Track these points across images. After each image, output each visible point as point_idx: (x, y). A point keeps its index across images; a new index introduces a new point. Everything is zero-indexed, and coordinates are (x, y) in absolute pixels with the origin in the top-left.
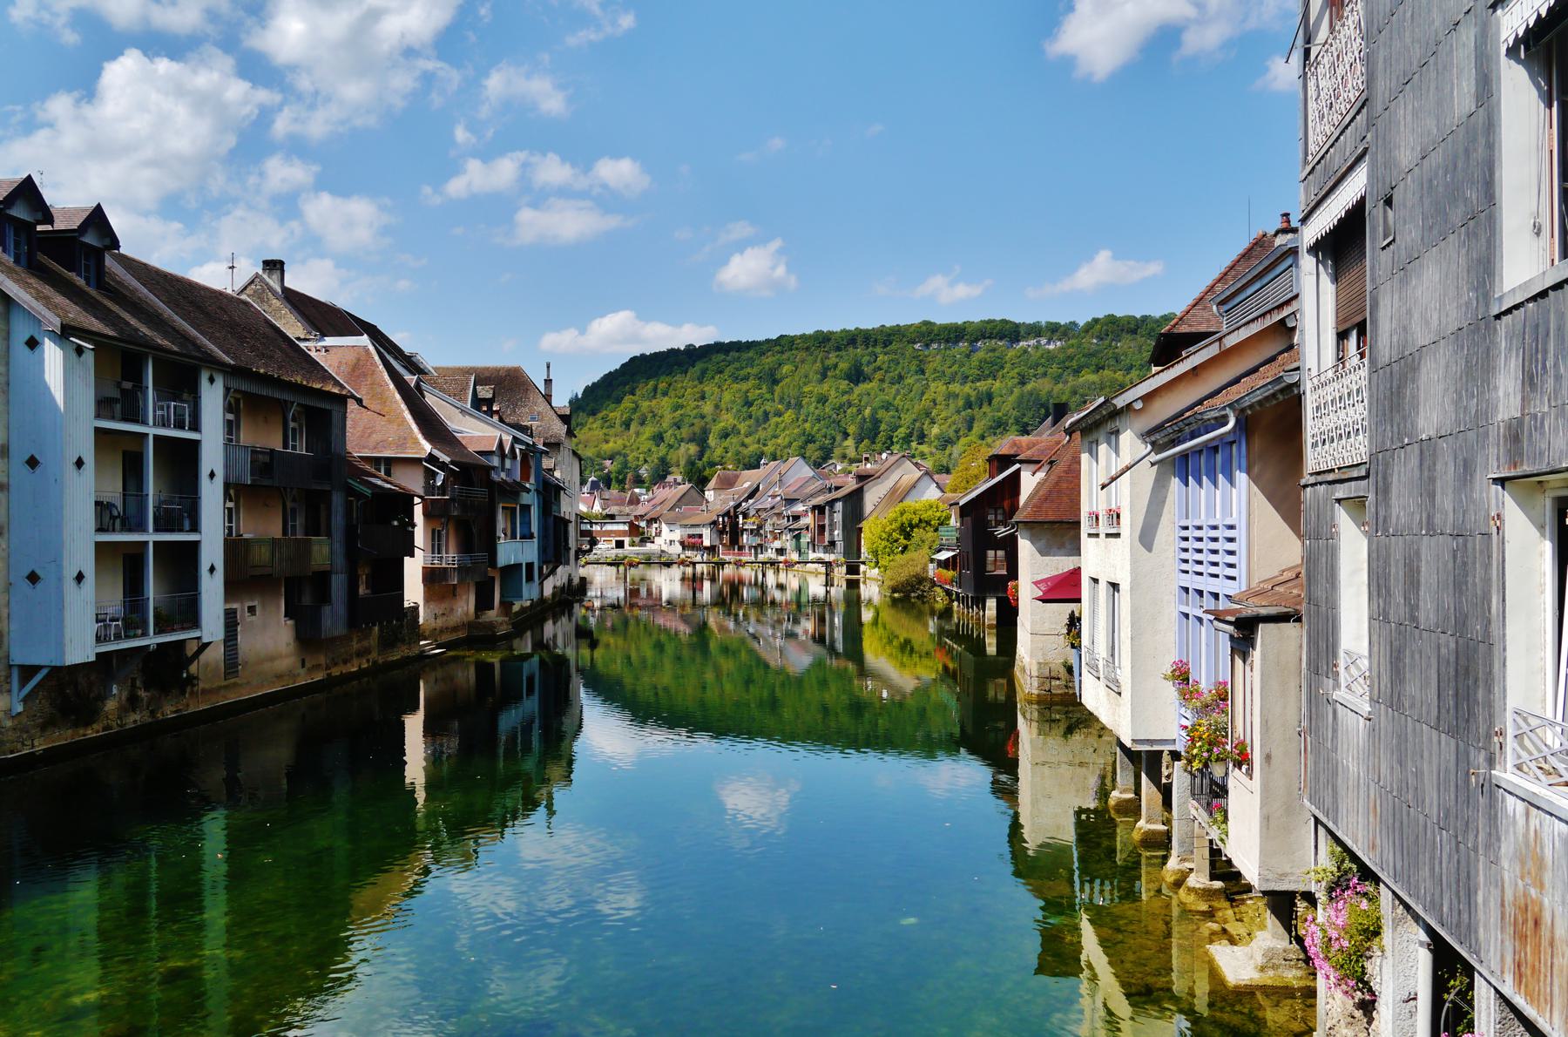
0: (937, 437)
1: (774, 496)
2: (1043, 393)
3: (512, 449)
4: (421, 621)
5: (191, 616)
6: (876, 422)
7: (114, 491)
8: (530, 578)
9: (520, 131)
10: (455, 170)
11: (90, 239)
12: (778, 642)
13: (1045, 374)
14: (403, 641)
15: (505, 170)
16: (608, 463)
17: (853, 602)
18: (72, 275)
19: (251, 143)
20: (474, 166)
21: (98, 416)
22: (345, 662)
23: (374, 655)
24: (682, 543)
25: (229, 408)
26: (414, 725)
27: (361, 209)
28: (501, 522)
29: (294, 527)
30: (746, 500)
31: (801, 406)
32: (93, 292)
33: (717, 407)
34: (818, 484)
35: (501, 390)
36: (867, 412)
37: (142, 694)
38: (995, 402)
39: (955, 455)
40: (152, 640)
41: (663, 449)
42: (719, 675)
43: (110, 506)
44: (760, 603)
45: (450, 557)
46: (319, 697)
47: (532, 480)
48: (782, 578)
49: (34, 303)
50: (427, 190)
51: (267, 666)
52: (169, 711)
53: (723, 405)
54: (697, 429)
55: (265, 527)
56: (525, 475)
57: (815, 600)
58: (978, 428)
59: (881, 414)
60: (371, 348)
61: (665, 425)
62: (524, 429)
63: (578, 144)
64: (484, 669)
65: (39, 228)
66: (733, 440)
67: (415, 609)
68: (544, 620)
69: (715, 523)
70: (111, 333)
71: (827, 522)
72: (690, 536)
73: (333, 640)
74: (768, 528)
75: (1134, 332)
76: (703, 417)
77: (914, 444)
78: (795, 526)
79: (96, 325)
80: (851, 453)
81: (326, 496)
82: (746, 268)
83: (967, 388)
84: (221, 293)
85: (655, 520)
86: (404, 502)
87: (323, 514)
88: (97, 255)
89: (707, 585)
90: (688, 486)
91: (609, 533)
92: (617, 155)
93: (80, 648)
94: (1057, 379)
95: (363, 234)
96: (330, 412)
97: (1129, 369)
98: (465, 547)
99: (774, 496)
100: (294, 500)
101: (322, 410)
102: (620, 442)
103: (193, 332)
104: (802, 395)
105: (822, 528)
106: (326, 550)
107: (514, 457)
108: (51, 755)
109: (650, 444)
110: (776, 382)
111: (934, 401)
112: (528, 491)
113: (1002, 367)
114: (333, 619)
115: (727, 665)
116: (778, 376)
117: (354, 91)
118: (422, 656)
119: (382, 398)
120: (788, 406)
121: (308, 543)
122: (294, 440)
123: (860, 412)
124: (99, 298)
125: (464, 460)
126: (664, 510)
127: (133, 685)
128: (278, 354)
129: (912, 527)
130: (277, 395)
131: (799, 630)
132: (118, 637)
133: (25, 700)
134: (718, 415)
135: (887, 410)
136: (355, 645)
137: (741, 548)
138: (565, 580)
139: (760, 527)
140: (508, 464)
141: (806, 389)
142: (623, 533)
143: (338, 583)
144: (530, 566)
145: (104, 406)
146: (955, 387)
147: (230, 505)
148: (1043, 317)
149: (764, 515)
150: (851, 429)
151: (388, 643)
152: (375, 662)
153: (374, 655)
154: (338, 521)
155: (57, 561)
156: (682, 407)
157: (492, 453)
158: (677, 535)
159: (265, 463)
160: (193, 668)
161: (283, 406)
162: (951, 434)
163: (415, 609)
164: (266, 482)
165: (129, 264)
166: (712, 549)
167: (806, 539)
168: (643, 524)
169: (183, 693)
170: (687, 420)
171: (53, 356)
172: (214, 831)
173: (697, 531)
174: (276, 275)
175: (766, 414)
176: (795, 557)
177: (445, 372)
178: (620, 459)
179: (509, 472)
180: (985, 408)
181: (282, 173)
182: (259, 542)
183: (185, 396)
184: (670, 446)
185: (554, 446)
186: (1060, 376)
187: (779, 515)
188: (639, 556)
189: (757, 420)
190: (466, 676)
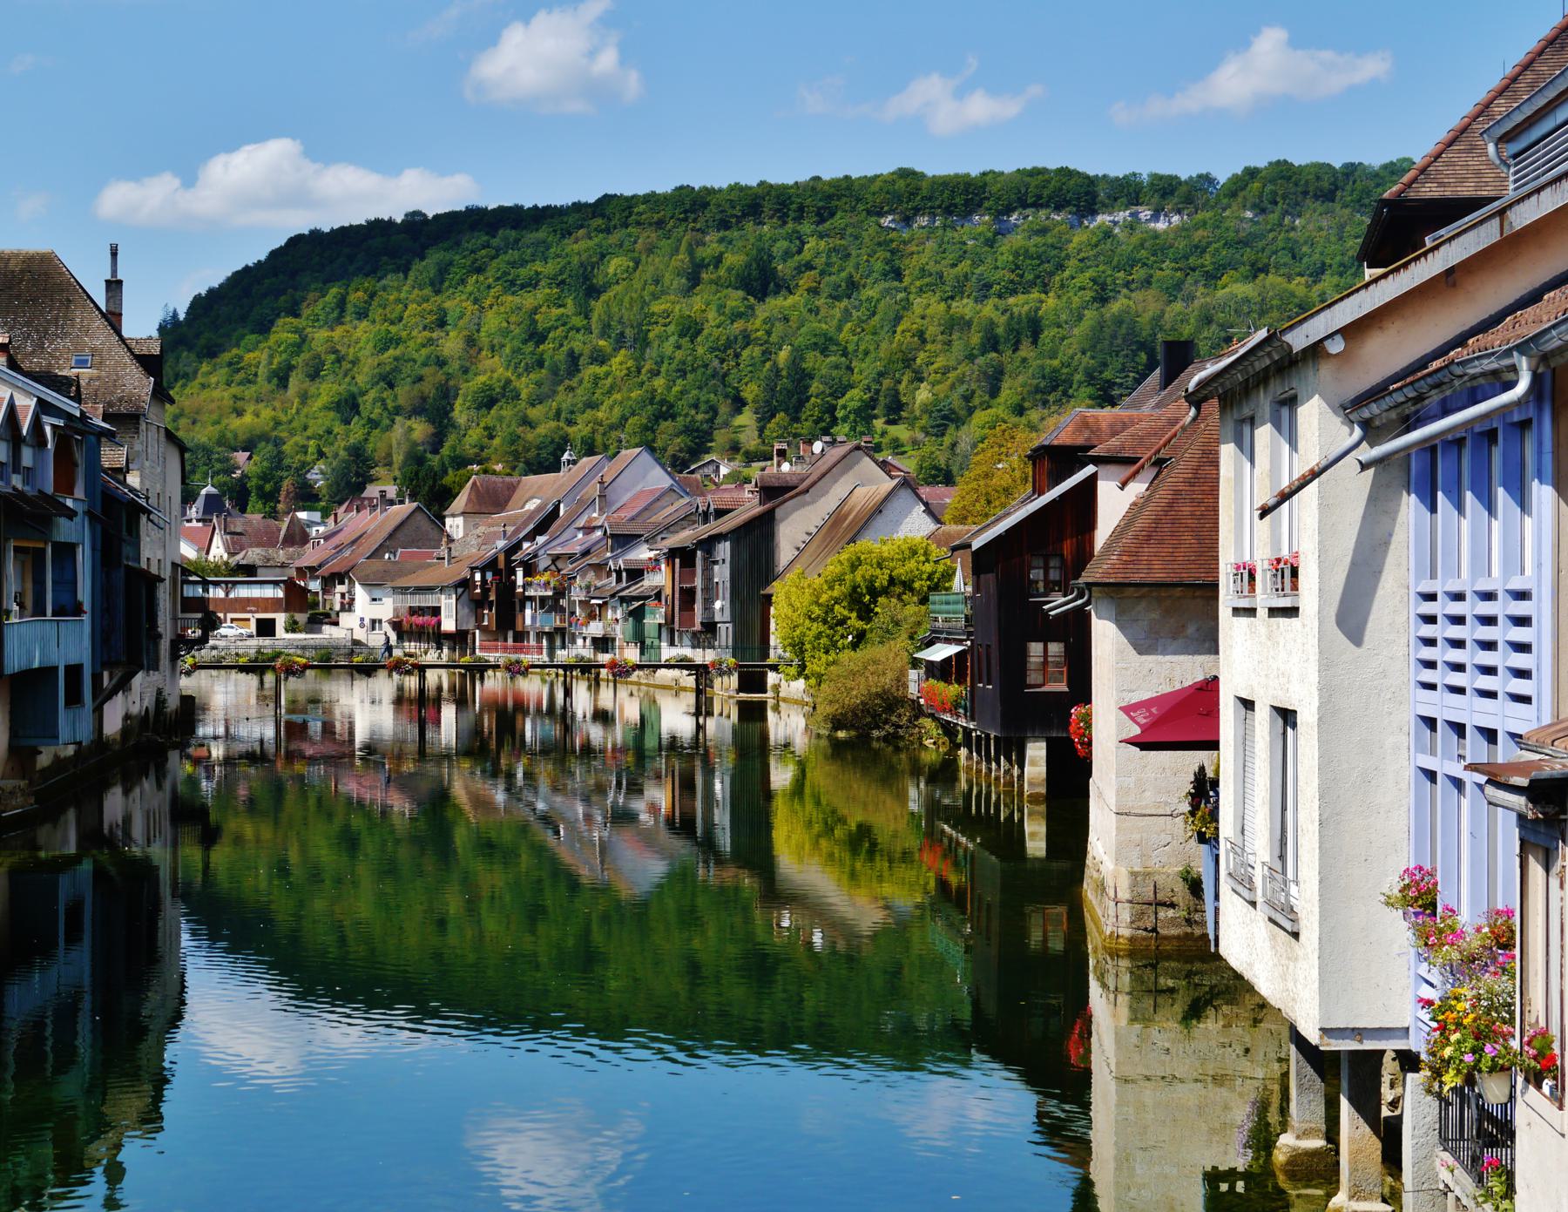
0: (926, 409)
1: (588, 530)
2: (1145, 319)
3: (37, 425)
6: (801, 377)
8: (74, 698)
13: (1147, 282)
16: (241, 457)
17: (752, 745)
21: (68, 668)
24: (396, 625)
30: (531, 537)
31: (646, 343)
33: (471, 342)
34: (681, 504)
36: (783, 356)
38: (1047, 335)
39: (963, 446)
41: (357, 431)
42: (472, 906)
44: (564, 750)
47: (79, 492)
48: (606, 698)
54: (428, 388)
56: (65, 482)
59: (812, 360)
61: (361, 380)
66: (506, 411)
69: (465, 584)
71: (698, 582)
72: (413, 611)
74: (577, 594)
75: (1328, 196)
76: (441, 363)
77: (879, 424)
78: (634, 591)
80: (750, 440)
83: (988, 309)
85: (340, 577)
89: (448, 713)
90: (409, 506)
91: (243, 605)
94: (1173, 291)
97: (1318, 273)
99: (588, 530)
105: (688, 597)
109: (330, 419)
110: (594, 292)
111: (921, 335)
112: (71, 514)
113: (1061, 267)
115: (492, 878)
116: (599, 280)
120: (620, 342)
123: (767, 355)
129: (875, 593)
131: (639, 805)
135: (824, 351)
137: (520, 637)
138: (149, 701)
139: (560, 593)
141: (656, 307)
142: (273, 604)
144: (74, 671)
146: (964, 307)
148: (1144, 164)
149: (567, 568)
150: (750, 391)
156: (398, 341)
158: (386, 609)
162: (956, 402)
166: (460, 639)
167: (655, 618)
168: (315, 586)
170: (407, 369)
173: (428, 601)
175: (573, 358)
176: (632, 655)
178: (266, 449)
179: (28, 474)
180: (1026, 351)
184: (373, 424)
185: (126, 420)
186: (1178, 286)
187: (599, 568)
189: (555, 371)
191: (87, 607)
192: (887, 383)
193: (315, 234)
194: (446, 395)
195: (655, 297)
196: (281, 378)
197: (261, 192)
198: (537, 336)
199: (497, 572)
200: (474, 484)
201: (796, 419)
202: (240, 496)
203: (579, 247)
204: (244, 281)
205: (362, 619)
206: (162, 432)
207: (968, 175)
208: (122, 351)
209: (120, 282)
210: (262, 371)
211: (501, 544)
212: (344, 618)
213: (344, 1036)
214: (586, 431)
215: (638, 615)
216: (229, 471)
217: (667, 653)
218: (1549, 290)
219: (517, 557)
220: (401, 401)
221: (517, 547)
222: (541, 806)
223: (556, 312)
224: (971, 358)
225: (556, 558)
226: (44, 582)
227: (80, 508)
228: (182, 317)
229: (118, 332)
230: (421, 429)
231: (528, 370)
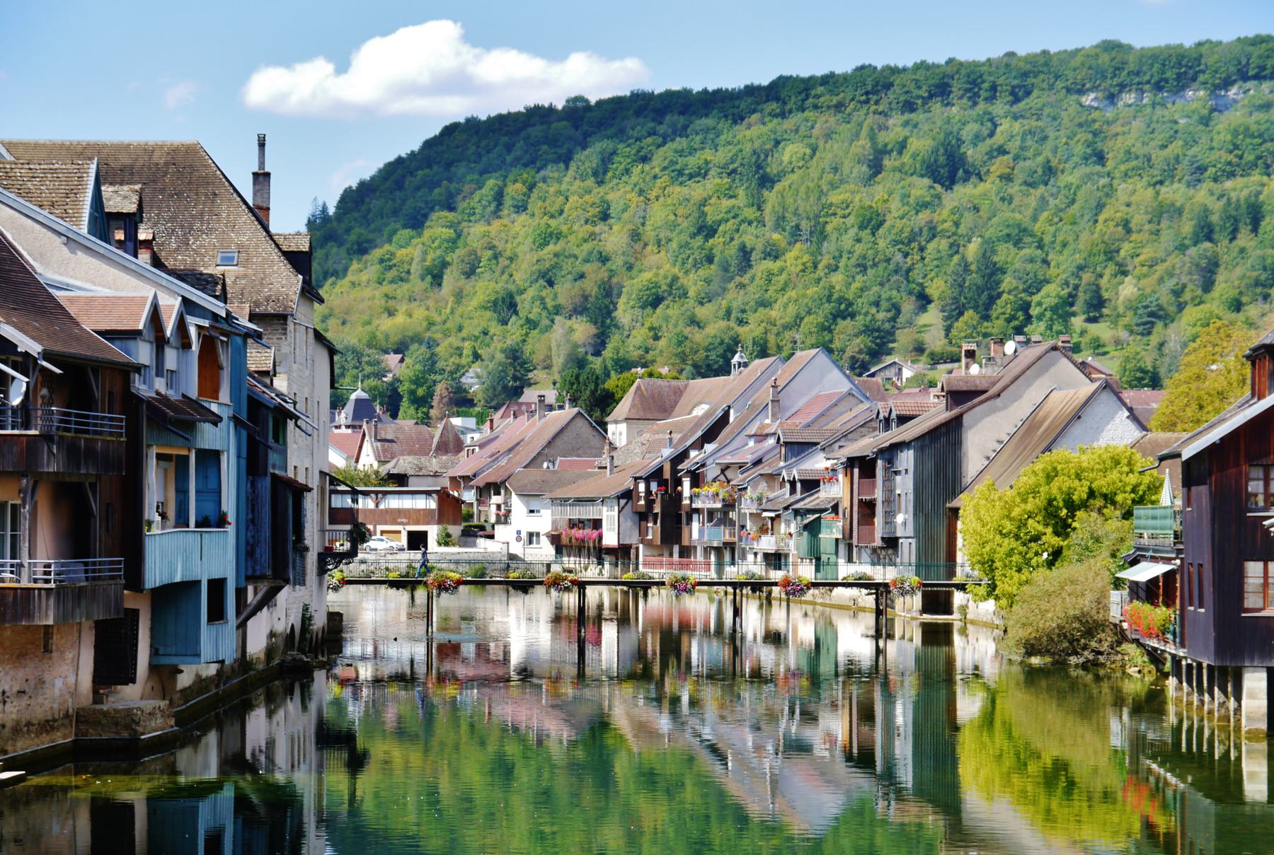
0: (1132, 307)
1: (761, 437)
3: (181, 326)
6: (992, 272)
8: (217, 614)
16: (392, 359)
17: (938, 678)
21: (211, 582)
24: (555, 540)
30: (699, 444)
31: (823, 236)
33: (635, 236)
35: (145, 198)
39: (1172, 345)
41: (515, 330)
44: (730, 675)
47: (225, 396)
48: (778, 619)
53: (649, 233)
56: (209, 385)
58: (1225, 285)
59: (1005, 252)
66: (671, 311)
69: (628, 495)
72: (573, 524)
74: (747, 506)
76: (604, 259)
78: (809, 503)
83: (1203, 195)
85: (494, 487)
98: (76, 542)
104: (828, 210)
107: (186, 345)
109: (487, 319)
110: (766, 181)
111: (1126, 225)
112: (216, 420)
116: (772, 169)
123: (955, 248)
129: (1072, 507)
131: (814, 736)
134: (638, 256)
135: (1018, 243)
137: (686, 552)
138: (295, 619)
141: (835, 197)
142: (425, 516)
144: (217, 586)
149: (737, 478)
150: (936, 288)
156: (558, 236)
157: (134, 334)
158: (544, 521)
162: (1165, 297)
166: (622, 553)
167: (832, 531)
170: (567, 265)
173: (589, 513)
175: (745, 254)
176: (807, 572)
184: (532, 324)
187: (771, 477)
191: (231, 518)
192: (1087, 277)
194: (609, 292)
195: (834, 187)
196: (436, 276)
198: (707, 230)
199: (662, 483)
200: (639, 388)
201: (986, 318)
204: (397, 172)
205: (519, 532)
206: (311, 333)
207: (1181, 46)
208: (270, 247)
209: (268, 175)
211: (667, 452)
212: (500, 531)
215: (813, 529)
216: (380, 375)
217: (845, 570)
219: (684, 466)
220: (562, 300)
221: (683, 455)
223: (727, 203)
224: (1182, 248)
225: (725, 468)
226: (186, 492)
227: (225, 413)
228: (331, 211)
230: (582, 330)
231: (696, 265)
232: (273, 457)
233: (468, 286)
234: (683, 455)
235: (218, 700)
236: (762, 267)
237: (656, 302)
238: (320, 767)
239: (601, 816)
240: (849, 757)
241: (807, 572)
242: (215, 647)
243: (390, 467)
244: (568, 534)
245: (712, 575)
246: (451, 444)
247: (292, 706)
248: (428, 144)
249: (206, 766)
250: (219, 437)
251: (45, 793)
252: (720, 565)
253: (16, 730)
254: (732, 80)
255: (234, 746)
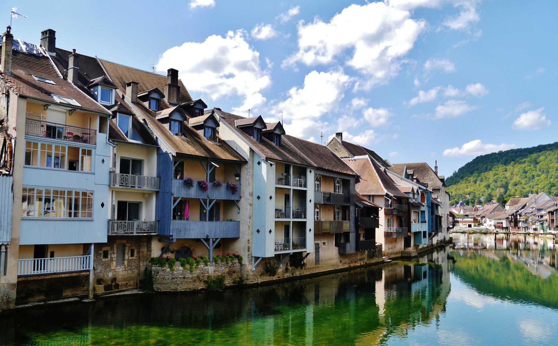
1: (532, 208)
3: (417, 191)
4: (383, 250)
5: (303, 244)
7: (281, 206)
8: (425, 237)
9: (439, 79)
10: (416, 95)
11: (277, 132)
12: (535, 266)
14: (376, 256)
15: (433, 93)
16: (468, 196)
18: (272, 143)
19: (347, 94)
20: (421, 93)
22: (355, 262)
23: (366, 261)
24: (495, 226)
25: (317, 179)
26: (380, 286)
27: (382, 112)
28: (413, 217)
29: (338, 218)
30: (521, 209)
31: (549, 172)
32: (277, 147)
33: (512, 174)
34: (552, 203)
35: (416, 172)
37: (289, 268)
40: (291, 251)
41: (490, 190)
42: (514, 278)
43: (280, 210)
44: (527, 249)
45: (394, 228)
46: (346, 273)
47: (426, 202)
48: (536, 240)
49: (259, 152)
50: (404, 103)
51: (329, 262)
52: (297, 273)
53: (514, 173)
54: (504, 183)
55: (327, 217)
56: (423, 200)
57: (550, 250)
60: (369, 159)
61: (490, 182)
62: (423, 184)
63: (460, 81)
64: (407, 268)
65: (263, 130)
66: (519, 186)
67: (381, 246)
68: (433, 252)
69: (508, 218)
70: (280, 159)
72: (498, 223)
73: (351, 254)
74: (530, 220)
76: (506, 178)
78: (542, 219)
79: (276, 157)
81: (348, 208)
82: (526, 120)
84: (317, 145)
85: (484, 217)
86: (375, 210)
87: (347, 214)
88: (279, 136)
89: (505, 242)
90: (497, 204)
91: (466, 222)
92: (475, 83)
93: (270, 253)
95: (382, 120)
96: (349, 180)
98: (400, 225)
99: (532, 208)
100: (338, 209)
101: (348, 180)
102: (472, 188)
103: (306, 157)
104: (550, 168)
106: (348, 225)
107: (418, 194)
108: (263, 284)
109: (485, 189)
110: (537, 163)
112: (424, 206)
114: (350, 247)
115: (518, 274)
116: (538, 161)
117: (380, 74)
118: (383, 262)
119: (372, 175)
120: (543, 172)
121: (342, 223)
122: (339, 189)
124: (279, 149)
125: (399, 195)
126: (487, 213)
127: (287, 265)
128: (333, 163)
130: (332, 175)
131: (543, 261)
132: (281, 250)
133: (256, 267)
134: (513, 177)
136: (359, 257)
137: (519, 228)
138: (442, 238)
139: (527, 220)
140: (416, 196)
141: (551, 165)
142: (471, 222)
143: (352, 236)
144: (425, 232)
145: (279, 180)
147: (317, 210)
149: (528, 215)
151: (371, 256)
152: (366, 263)
153: (366, 261)
154: (352, 216)
155: (264, 226)
156: (497, 174)
157: (409, 193)
158: (493, 223)
159: (328, 198)
160: (305, 261)
161: (334, 179)
163: (381, 246)
164: (328, 203)
165: (289, 137)
166: (507, 228)
167: (546, 224)
168: (479, 218)
169: (302, 268)
170: (499, 179)
171: (264, 165)
172: (310, 312)
173: (500, 221)
174: (340, 137)
175: (533, 176)
176: (542, 232)
177: (396, 165)
178: (472, 194)
179: (416, 199)
181: (357, 102)
182: (326, 222)
183: (302, 177)
184: (493, 189)
185: (437, 190)
187: (535, 215)
188: (475, 230)
189: (529, 178)
190: (400, 270)
191: (427, 221)
193: (481, 156)
194: (507, 184)
195: (550, 163)
196: (475, 182)
197: (472, 149)
198: (526, 172)
199: (514, 216)
202: (468, 203)
203: (534, 155)
204: (468, 165)
210: (472, 181)
211: (515, 211)
212: (484, 224)
213: (491, 301)
214: (536, 190)
215: (542, 224)
216: (465, 198)
217: (548, 231)
218: (325, 169)
219: (518, 213)
220: (498, 185)
221: (518, 211)
222: (523, 259)
223: (529, 167)
225: (526, 214)
229: (437, 175)
230: (502, 190)
231: (524, 178)
232: (436, 212)
233: (481, 183)
234: (518, 211)
235: (427, 251)
236: (536, 178)
237: (516, 185)
238: (448, 262)
239: (508, 274)
240: (550, 265)
241: (542, 232)
242: (425, 243)
243: (466, 214)
244: (497, 225)
245: (524, 232)
246: (477, 210)
247: (442, 252)
248: (474, 160)
249: (425, 261)
250: (425, 208)
251: (396, 264)
252: (525, 230)
253: (391, 254)
254: (530, 146)
255: (430, 258)
